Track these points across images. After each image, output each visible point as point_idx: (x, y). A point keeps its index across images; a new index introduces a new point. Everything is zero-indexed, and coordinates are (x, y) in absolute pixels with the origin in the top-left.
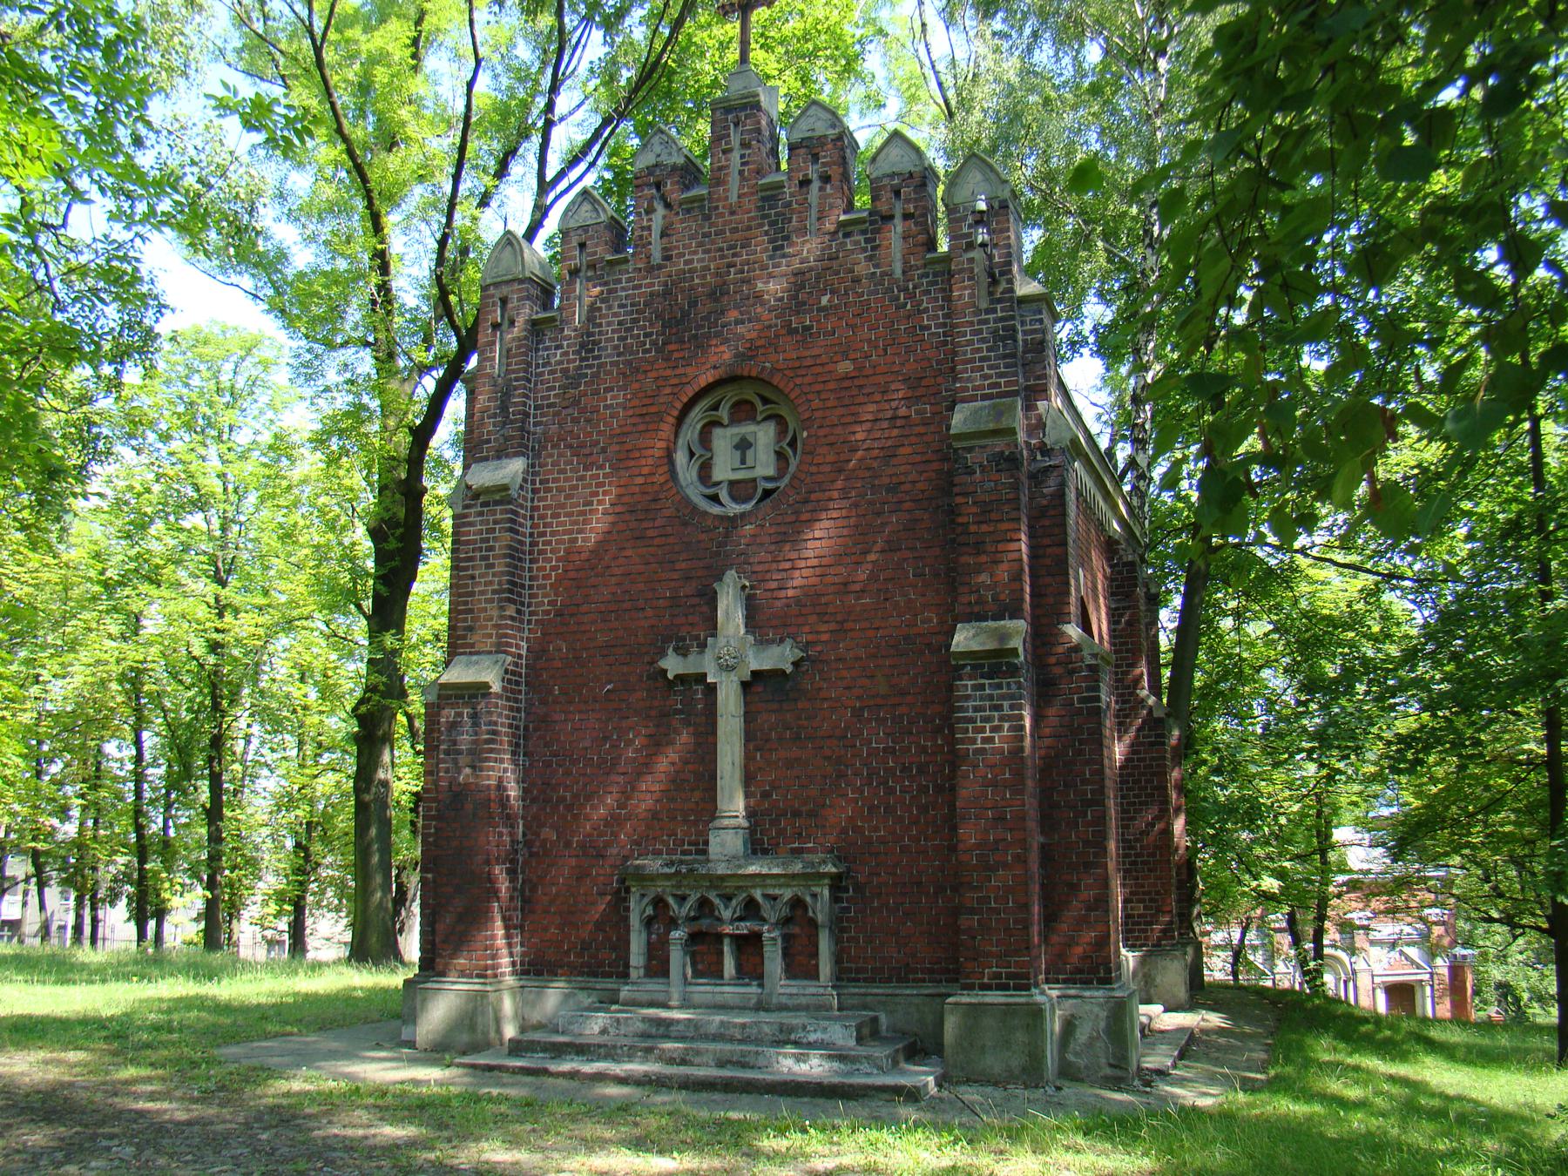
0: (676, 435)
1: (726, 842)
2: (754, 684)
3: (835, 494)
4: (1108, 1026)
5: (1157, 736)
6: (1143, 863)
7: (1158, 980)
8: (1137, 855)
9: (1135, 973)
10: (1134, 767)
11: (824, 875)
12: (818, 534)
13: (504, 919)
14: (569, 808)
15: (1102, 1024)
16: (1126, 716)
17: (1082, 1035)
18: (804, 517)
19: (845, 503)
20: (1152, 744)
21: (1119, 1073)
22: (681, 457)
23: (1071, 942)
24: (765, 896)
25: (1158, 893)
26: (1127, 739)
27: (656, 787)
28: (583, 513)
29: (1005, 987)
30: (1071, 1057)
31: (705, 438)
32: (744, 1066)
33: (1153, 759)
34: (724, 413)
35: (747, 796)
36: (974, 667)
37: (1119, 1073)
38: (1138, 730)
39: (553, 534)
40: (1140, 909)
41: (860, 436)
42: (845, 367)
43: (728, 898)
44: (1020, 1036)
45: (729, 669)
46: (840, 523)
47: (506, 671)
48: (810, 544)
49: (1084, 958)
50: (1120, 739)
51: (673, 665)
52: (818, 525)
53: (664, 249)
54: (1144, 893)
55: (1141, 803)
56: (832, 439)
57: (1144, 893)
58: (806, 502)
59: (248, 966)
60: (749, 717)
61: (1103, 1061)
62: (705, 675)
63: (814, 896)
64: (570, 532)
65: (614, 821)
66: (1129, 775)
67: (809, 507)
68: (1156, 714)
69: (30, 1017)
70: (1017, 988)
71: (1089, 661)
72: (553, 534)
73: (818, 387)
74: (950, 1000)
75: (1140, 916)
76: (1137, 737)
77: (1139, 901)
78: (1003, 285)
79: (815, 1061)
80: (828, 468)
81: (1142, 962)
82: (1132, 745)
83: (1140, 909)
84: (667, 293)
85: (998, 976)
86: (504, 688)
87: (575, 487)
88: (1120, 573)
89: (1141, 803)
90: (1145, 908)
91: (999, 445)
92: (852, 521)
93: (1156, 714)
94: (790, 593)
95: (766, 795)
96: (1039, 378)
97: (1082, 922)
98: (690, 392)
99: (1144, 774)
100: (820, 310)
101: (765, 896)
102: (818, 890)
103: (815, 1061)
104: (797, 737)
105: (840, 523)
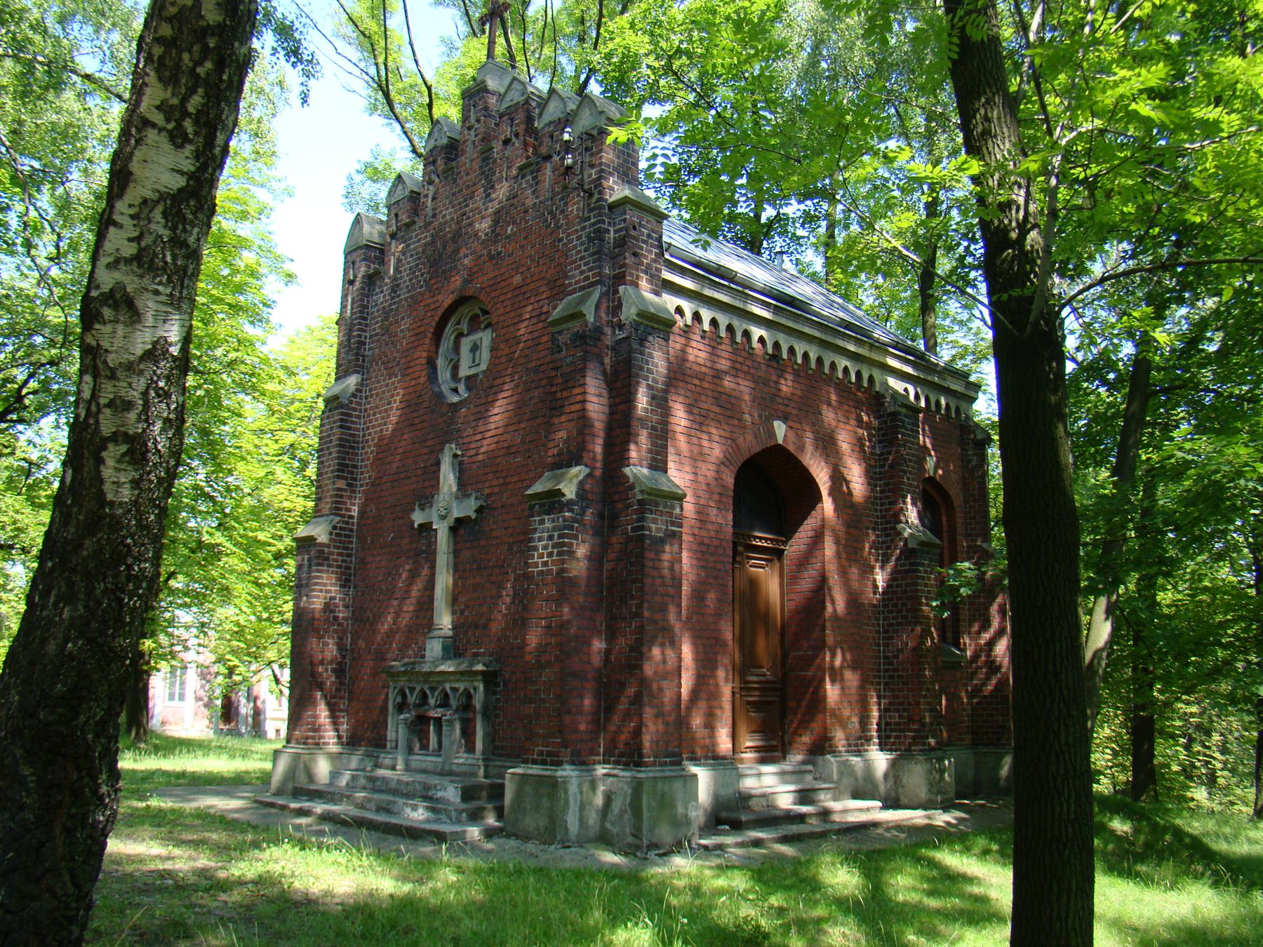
0: (437, 346)
1: (434, 648)
2: (458, 526)
3: (508, 379)
4: (632, 801)
5: (911, 564)
6: (899, 677)
7: (904, 781)
8: (894, 670)
9: (886, 776)
10: (893, 593)
11: (477, 672)
12: (496, 411)
13: (328, 704)
14: (371, 625)
15: (628, 800)
16: (888, 548)
17: (616, 807)
18: (490, 399)
19: (512, 385)
20: (907, 572)
21: (637, 842)
22: (440, 362)
23: (619, 731)
24: (452, 689)
25: (909, 704)
26: (889, 569)
27: (412, 608)
28: (386, 411)
29: (544, 763)
30: (608, 825)
31: (456, 348)
32: (389, 811)
33: (907, 585)
34: (464, 327)
35: (453, 613)
36: (541, 505)
37: (637, 842)
38: (897, 560)
39: (373, 427)
40: (895, 717)
41: (522, 332)
42: (517, 279)
43: (433, 689)
44: (545, 803)
45: (443, 518)
46: (509, 400)
47: (334, 528)
48: (492, 419)
49: (626, 744)
50: (882, 568)
51: (418, 518)
52: (498, 403)
53: (434, 209)
54: (900, 704)
55: (898, 624)
56: (507, 337)
57: (900, 704)
58: (491, 387)
59: (270, 741)
60: (456, 552)
61: (628, 830)
62: (431, 523)
63: (475, 689)
64: (379, 425)
65: (391, 633)
66: (889, 599)
67: (493, 390)
68: (910, 546)
69: (211, 773)
70: (552, 764)
71: (639, 497)
72: (373, 427)
73: (502, 298)
74: (510, 771)
75: (896, 724)
76: (896, 566)
77: (897, 711)
78: (596, 196)
79: (421, 811)
80: (504, 359)
81: (893, 764)
82: (892, 574)
83: (895, 717)
84: (433, 242)
85: (541, 753)
86: (331, 540)
87: (383, 393)
88: (885, 422)
89: (898, 624)
90: (900, 717)
91: (575, 326)
92: (515, 398)
93: (910, 546)
94: (480, 457)
95: (462, 612)
96: (621, 267)
97: (627, 716)
98: (440, 311)
99: (901, 598)
100: (508, 237)
101: (452, 689)
102: (476, 684)
103: (421, 811)
104: (479, 568)
105: (509, 400)
